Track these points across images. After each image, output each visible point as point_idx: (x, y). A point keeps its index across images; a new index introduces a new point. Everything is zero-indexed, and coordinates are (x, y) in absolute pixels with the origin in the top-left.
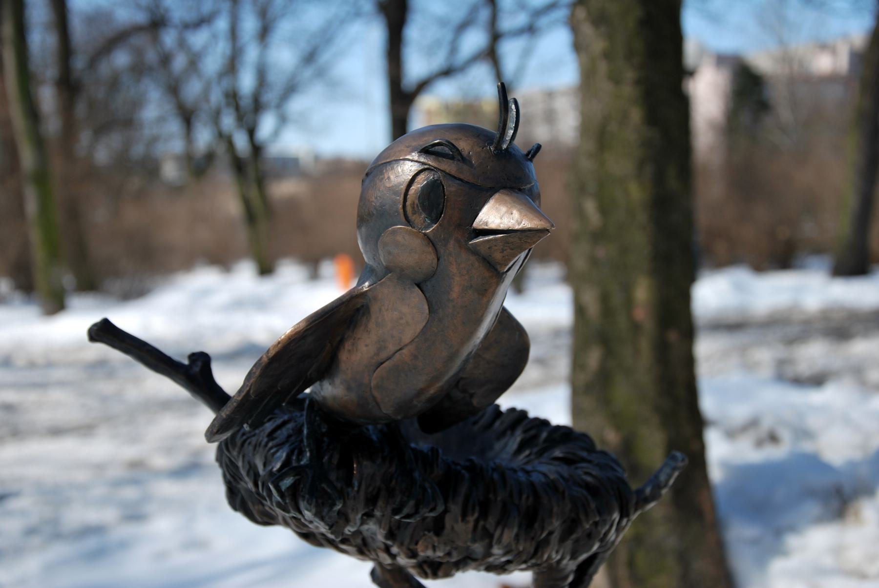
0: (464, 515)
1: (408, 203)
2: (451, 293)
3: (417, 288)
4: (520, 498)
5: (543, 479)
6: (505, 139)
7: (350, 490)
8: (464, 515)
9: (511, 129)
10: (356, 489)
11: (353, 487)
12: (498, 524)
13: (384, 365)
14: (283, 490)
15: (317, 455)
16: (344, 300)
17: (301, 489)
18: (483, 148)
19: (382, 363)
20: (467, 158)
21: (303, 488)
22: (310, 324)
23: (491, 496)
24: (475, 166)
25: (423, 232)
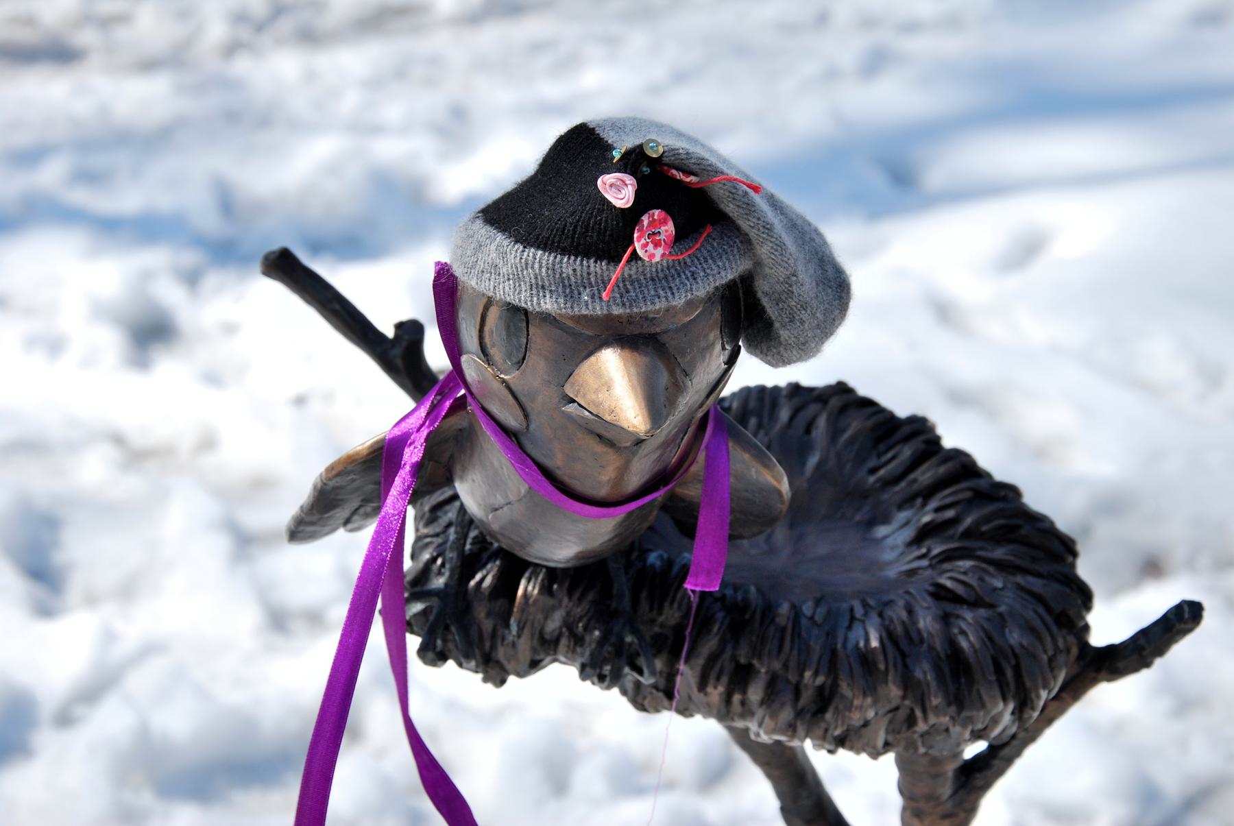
0: (702, 686)
1: (487, 329)
7: (507, 632)
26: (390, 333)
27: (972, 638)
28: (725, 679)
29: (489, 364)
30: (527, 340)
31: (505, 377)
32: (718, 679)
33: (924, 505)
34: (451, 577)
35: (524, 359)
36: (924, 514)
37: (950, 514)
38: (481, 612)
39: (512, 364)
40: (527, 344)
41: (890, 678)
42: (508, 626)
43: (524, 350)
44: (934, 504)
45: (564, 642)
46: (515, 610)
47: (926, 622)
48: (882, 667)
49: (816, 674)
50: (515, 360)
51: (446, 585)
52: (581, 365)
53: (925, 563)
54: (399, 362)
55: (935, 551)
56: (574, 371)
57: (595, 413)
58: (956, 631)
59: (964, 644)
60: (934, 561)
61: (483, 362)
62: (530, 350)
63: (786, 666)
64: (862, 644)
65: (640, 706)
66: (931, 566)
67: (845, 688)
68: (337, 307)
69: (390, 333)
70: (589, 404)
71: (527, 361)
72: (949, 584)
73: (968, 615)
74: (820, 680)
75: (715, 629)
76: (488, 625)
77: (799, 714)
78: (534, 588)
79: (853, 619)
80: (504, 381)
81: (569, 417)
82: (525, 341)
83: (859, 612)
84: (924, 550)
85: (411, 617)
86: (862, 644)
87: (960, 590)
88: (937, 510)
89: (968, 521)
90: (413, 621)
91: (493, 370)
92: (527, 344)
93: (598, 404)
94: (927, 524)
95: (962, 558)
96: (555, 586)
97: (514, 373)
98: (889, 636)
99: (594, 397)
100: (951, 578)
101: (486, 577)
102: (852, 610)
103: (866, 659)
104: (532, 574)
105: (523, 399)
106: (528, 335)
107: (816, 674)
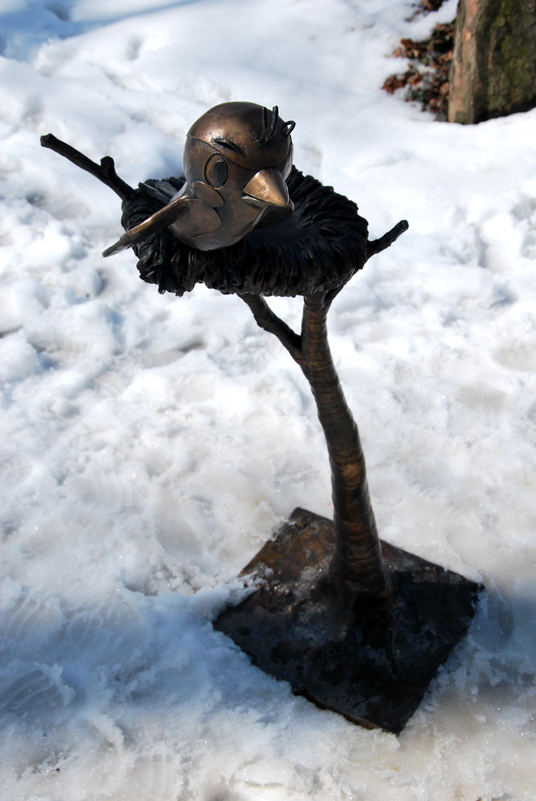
0: (254, 283)
1: (208, 171)
2: (216, 713)
3: (214, 210)
4: (289, 272)
5: (426, 708)
6: (283, 207)
7: (186, 276)
8: (254, 283)
9: (401, 565)
10: (189, 276)
11: (188, 276)
12: (275, 285)
13: (199, 236)
14: (172, 225)
15: (167, 259)
16: (174, 206)
17: (158, 277)
18: (253, 142)
19: (197, 235)
20: (242, 150)
21: (159, 276)
22: (154, 221)
23: (272, 271)
24: (246, 155)
25: (215, 188)
26: (99, 163)
27: (341, 248)
28: (263, 279)
29: (209, 185)
30: (227, 174)
31: (218, 189)
32: (260, 280)
33: (304, 200)
34: (164, 259)
35: (225, 182)
36: (306, 203)
37: (316, 202)
38: (176, 270)
39: (220, 184)
40: (227, 175)
41: (318, 268)
42: (186, 274)
43: (226, 178)
44: (308, 199)
45: (205, 276)
46: (189, 268)
47: (323, 245)
48: (316, 265)
49: (294, 272)
50: (222, 182)
51: (163, 262)
52: (250, 181)
53: (312, 222)
54: (106, 175)
55: (314, 217)
56: (247, 184)
57: (261, 199)
58: (334, 246)
59: (338, 251)
60: (315, 220)
61: (207, 184)
62: (229, 178)
63: (284, 271)
64: (307, 257)
65: (143, 277)
66: (313, 222)
67: (304, 274)
68: (77, 156)
69: (99, 163)
70: (257, 196)
71: (227, 182)
72: (326, 229)
73: (337, 240)
74: (296, 273)
75: (257, 262)
76: (179, 275)
77: (288, 287)
78: (194, 258)
79: (299, 248)
80: (216, 190)
81: (244, 201)
82: (226, 175)
83: (301, 246)
84: (310, 217)
85: (149, 277)
86: (307, 257)
87: (331, 231)
88: (310, 201)
89: (323, 204)
90: (150, 278)
91: (211, 187)
92: (227, 175)
93: (262, 196)
94: (308, 207)
95: (325, 218)
96: (201, 256)
97: (221, 187)
98: (315, 254)
99: (259, 193)
100: (325, 227)
101: (175, 259)
102: (297, 245)
103: (310, 262)
104: (191, 253)
105: (224, 196)
106: (227, 172)
107: (294, 272)
